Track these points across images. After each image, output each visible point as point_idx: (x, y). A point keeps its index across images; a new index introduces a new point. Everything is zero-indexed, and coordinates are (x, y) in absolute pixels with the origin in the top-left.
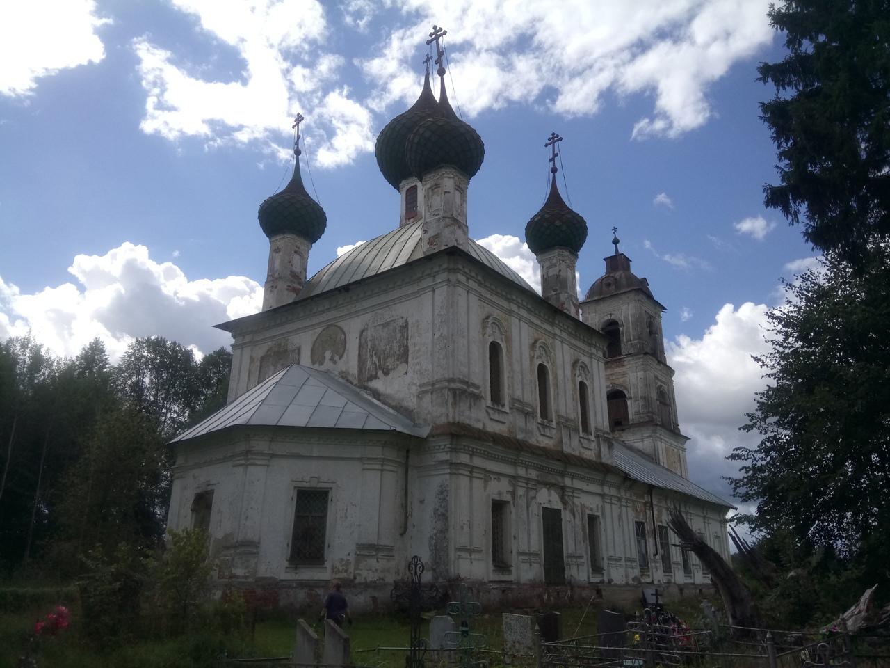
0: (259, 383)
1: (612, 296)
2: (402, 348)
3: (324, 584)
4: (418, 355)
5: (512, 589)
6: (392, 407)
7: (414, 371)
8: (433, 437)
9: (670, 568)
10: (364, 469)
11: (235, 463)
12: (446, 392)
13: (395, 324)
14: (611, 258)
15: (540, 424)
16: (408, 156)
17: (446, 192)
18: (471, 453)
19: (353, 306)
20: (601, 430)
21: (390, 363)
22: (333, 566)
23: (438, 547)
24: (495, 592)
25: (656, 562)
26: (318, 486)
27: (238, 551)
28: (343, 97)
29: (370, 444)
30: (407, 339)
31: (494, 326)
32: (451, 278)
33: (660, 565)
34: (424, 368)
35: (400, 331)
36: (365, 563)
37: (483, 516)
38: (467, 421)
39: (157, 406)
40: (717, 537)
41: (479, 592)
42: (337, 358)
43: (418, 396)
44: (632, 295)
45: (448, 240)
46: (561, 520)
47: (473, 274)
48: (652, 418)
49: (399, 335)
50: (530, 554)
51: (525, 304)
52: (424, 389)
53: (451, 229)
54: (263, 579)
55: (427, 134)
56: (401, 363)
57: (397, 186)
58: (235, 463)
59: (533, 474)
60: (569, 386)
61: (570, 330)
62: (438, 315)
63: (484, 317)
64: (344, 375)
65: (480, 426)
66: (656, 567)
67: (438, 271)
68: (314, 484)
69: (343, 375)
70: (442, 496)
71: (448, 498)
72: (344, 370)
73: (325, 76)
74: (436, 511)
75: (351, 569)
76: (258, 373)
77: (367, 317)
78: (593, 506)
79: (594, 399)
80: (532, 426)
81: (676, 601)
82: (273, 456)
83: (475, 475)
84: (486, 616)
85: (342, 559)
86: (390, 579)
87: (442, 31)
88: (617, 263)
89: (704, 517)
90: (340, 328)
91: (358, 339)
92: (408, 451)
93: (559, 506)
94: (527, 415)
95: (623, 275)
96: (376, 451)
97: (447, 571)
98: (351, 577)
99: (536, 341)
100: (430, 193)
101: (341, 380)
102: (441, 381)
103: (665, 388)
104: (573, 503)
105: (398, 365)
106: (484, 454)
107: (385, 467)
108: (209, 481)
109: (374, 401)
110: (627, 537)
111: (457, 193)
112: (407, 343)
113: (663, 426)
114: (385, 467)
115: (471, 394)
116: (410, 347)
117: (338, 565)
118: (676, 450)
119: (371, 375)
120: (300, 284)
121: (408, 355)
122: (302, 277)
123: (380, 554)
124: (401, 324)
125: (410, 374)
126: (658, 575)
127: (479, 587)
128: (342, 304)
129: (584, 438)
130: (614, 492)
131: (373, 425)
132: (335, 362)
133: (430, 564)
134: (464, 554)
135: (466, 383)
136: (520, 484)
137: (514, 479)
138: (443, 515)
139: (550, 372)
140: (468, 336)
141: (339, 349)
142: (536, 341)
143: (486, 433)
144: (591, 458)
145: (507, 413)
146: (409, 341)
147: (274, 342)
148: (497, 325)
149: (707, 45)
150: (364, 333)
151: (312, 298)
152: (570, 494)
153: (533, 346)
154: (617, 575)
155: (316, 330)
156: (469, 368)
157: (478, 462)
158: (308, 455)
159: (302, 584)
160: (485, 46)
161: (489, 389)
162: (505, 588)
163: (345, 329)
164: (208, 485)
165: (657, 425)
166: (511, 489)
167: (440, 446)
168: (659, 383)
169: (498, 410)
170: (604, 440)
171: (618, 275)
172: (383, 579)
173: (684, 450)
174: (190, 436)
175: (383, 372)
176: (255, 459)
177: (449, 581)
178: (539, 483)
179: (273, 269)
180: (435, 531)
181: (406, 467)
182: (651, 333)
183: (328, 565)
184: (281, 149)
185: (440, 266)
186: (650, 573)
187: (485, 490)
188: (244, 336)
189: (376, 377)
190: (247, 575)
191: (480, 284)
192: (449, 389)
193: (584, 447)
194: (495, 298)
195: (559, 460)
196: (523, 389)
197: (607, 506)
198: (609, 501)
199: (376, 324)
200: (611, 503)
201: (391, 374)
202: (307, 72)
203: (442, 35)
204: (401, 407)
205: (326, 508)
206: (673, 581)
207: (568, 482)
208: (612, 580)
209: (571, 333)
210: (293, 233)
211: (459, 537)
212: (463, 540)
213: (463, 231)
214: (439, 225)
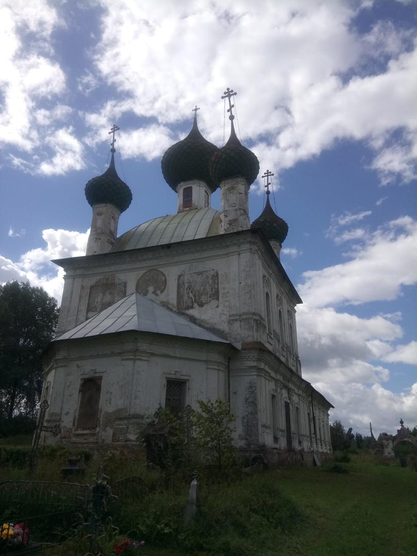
2: (214, 290)
7: (224, 306)
8: (245, 350)
10: (207, 368)
17: (240, 193)
27: (131, 422)
28: (68, 134)
30: (218, 284)
34: (233, 304)
42: (158, 292)
49: (211, 281)
56: (213, 299)
62: (243, 271)
68: (178, 376)
69: (165, 304)
71: (256, 391)
72: (165, 300)
73: (58, 117)
74: (246, 399)
76: (88, 297)
77: (183, 267)
82: (152, 354)
87: (233, 93)
90: (160, 272)
91: (177, 281)
92: (229, 358)
96: (214, 357)
97: (258, 440)
100: (228, 193)
105: (210, 301)
108: (96, 370)
112: (218, 286)
116: (220, 290)
120: (114, 239)
121: (219, 295)
124: (213, 274)
125: (221, 307)
128: (163, 256)
132: (157, 295)
133: (243, 435)
138: (252, 402)
141: (161, 286)
146: (219, 286)
149: (285, 149)
154: (267, 440)
155: (141, 272)
160: (164, 122)
163: (165, 273)
164: (96, 373)
167: (249, 356)
175: (198, 305)
179: (96, 226)
180: (246, 413)
181: (228, 369)
184: (15, 159)
188: (75, 270)
189: (192, 307)
199: (191, 272)
202: (47, 113)
203: (233, 95)
204: (215, 329)
210: (112, 204)
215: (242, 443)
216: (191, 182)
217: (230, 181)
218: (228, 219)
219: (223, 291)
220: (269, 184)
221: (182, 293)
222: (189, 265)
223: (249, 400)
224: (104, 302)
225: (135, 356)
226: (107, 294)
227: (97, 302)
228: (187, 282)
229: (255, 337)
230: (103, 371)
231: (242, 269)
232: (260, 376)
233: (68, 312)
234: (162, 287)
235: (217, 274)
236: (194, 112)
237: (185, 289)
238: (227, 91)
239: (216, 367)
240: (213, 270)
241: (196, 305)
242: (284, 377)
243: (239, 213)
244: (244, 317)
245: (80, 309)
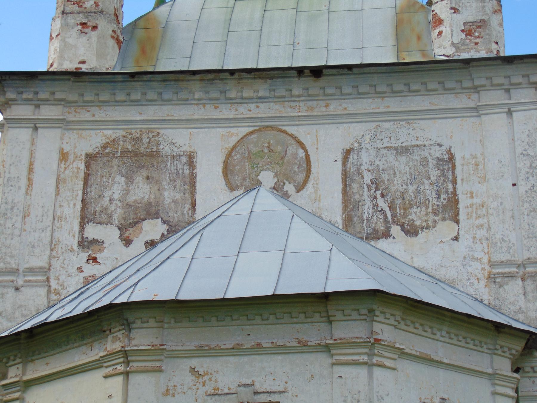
2: (444, 196)
4: (479, 212)
7: (474, 238)
10: (494, 393)
13: (425, 153)
19: (322, 103)
30: (454, 182)
34: (498, 236)
42: (289, 188)
49: (434, 174)
56: (444, 219)
58: (336, 358)
67: (47, 100)
82: (402, 354)
90: (292, 136)
91: (340, 164)
107: (500, 389)
112: (455, 188)
119: (375, 231)
124: (438, 155)
125: (465, 241)
128: (299, 96)
146: (458, 186)
150: (353, 157)
155: (234, 130)
164: (256, 393)
175: (403, 229)
189: (386, 235)
199: (380, 146)
201: (421, 235)
214: (483, 7)
218: (460, 19)
219: (470, 201)
222: (373, 125)
224: (131, 199)
225: (371, 355)
226: (139, 179)
227: (111, 200)
230: (274, 389)
231: (519, 150)
233: (24, 217)
234: (301, 177)
235: (452, 158)
237: (366, 188)
241: (395, 230)
244: (530, 269)
245: (59, 214)
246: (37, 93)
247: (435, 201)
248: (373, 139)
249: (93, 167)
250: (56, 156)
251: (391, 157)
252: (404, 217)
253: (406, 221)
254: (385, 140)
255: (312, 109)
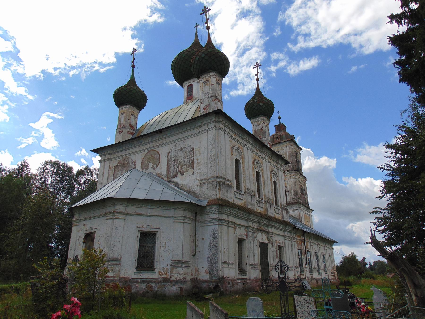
0: (113, 180)
1: (279, 143)
2: (191, 161)
3: (156, 281)
5: (247, 283)
6: (186, 191)
8: (209, 206)
9: (312, 271)
10: (174, 222)
11: (107, 218)
12: (215, 183)
13: (187, 149)
14: (278, 125)
15: (257, 201)
16: (193, 67)
17: (212, 84)
18: (228, 214)
19: (164, 140)
20: (283, 205)
21: (184, 169)
22: (159, 272)
23: (212, 262)
24: (240, 284)
25: (306, 268)
26: (151, 230)
29: (178, 209)
30: (193, 157)
31: (237, 151)
32: (216, 126)
33: (308, 270)
34: (203, 171)
35: (190, 153)
36: (176, 270)
37: (234, 245)
38: (226, 198)
39: (54, 194)
40: (330, 256)
41: (233, 284)
42: (155, 167)
43: (200, 186)
44: (288, 143)
45: (214, 107)
46: (268, 248)
47: (227, 124)
48: (298, 201)
49: (189, 155)
50: (254, 265)
51: (250, 141)
52: (203, 182)
53: (215, 102)
54: (122, 278)
55: (203, 56)
56: (190, 169)
57: (181, 84)
58: (107, 218)
59: (255, 225)
60: (269, 183)
61: (269, 155)
63: (232, 146)
64: (159, 175)
65: (231, 201)
66: (307, 271)
68: (149, 229)
69: (159, 175)
70: (214, 236)
71: (217, 237)
72: (159, 172)
75: (169, 273)
77: (171, 146)
78: (281, 242)
79: (280, 189)
80: (255, 202)
81: (315, 286)
82: (127, 214)
83: (230, 225)
84: (237, 296)
85: (164, 268)
86: (188, 278)
87: (208, 9)
88: (280, 128)
89: (325, 247)
90: (156, 151)
91: (167, 157)
92: (196, 213)
93: (266, 241)
94: (252, 196)
95: (284, 133)
96: (180, 213)
97: (218, 274)
98: (169, 277)
99: (255, 160)
101: (157, 178)
102: (212, 178)
103: (303, 186)
104: (272, 240)
105: (188, 170)
106: (234, 215)
107: (185, 221)
109: (176, 188)
110: (295, 257)
111: (217, 85)
112: (193, 158)
113: (302, 204)
114: (185, 221)
115: (227, 184)
117: (162, 271)
118: (308, 216)
119: (174, 175)
120: (134, 130)
122: (135, 127)
123: (183, 265)
125: (195, 174)
126: (307, 274)
127: (233, 281)
129: (276, 208)
130: (289, 234)
131: (179, 199)
132: (154, 169)
134: (226, 266)
135: (225, 179)
136: (250, 230)
137: (247, 227)
138: (215, 246)
139: (261, 175)
140: (225, 155)
141: (157, 162)
142: (255, 160)
143: (235, 205)
144: (279, 218)
145: (243, 195)
146: (194, 158)
147: (122, 159)
148: (238, 151)
150: (170, 154)
151: (142, 136)
152: (271, 235)
153: (254, 162)
155: (144, 153)
156: (226, 172)
157: (231, 219)
158: (146, 214)
159: (144, 281)
161: (235, 182)
162: (245, 282)
164: (92, 229)
165: (300, 204)
166: (246, 233)
167: (213, 211)
168: (301, 185)
169: (239, 193)
170: (284, 210)
171: (281, 133)
172: (185, 278)
173: (311, 216)
174: (82, 204)
176: (118, 216)
177: (219, 279)
178: (258, 230)
180: (210, 254)
181: (195, 220)
182: (297, 161)
183: (157, 271)
185: (211, 119)
186: (304, 274)
187: (234, 233)
189: (176, 176)
190: (114, 276)
191: (230, 130)
192: (217, 182)
193: (276, 213)
194: (236, 137)
195: (267, 219)
196: (250, 183)
197: (286, 241)
198: (287, 239)
199: (176, 149)
200: (288, 240)
204: (191, 191)
205: (155, 242)
206: (313, 277)
207: (270, 229)
208: (289, 277)
209: (269, 157)
211: (223, 257)
212: (225, 259)
213: (221, 104)
215: (207, 277)
216: (192, 80)
217: (205, 76)
219: (197, 162)
220: (258, 73)
221: (170, 166)
222: (175, 144)
223: (213, 244)
228: (173, 157)
229: (218, 195)
231: (209, 143)
232: (221, 225)
235: (193, 149)
236: (196, 28)
238: (204, 9)
239: (182, 221)
240: (190, 146)
242: (258, 223)
243: (210, 99)
246: (104, 153)
247: (188, 164)
248: (175, 148)
249: (116, 169)
250: (108, 168)
251: (179, 152)
252: (181, 170)
253: (181, 171)
254: (178, 147)
255: (161, 142)
